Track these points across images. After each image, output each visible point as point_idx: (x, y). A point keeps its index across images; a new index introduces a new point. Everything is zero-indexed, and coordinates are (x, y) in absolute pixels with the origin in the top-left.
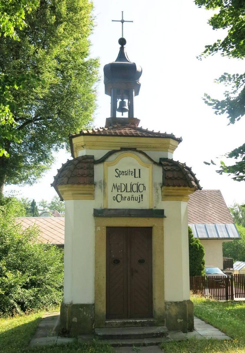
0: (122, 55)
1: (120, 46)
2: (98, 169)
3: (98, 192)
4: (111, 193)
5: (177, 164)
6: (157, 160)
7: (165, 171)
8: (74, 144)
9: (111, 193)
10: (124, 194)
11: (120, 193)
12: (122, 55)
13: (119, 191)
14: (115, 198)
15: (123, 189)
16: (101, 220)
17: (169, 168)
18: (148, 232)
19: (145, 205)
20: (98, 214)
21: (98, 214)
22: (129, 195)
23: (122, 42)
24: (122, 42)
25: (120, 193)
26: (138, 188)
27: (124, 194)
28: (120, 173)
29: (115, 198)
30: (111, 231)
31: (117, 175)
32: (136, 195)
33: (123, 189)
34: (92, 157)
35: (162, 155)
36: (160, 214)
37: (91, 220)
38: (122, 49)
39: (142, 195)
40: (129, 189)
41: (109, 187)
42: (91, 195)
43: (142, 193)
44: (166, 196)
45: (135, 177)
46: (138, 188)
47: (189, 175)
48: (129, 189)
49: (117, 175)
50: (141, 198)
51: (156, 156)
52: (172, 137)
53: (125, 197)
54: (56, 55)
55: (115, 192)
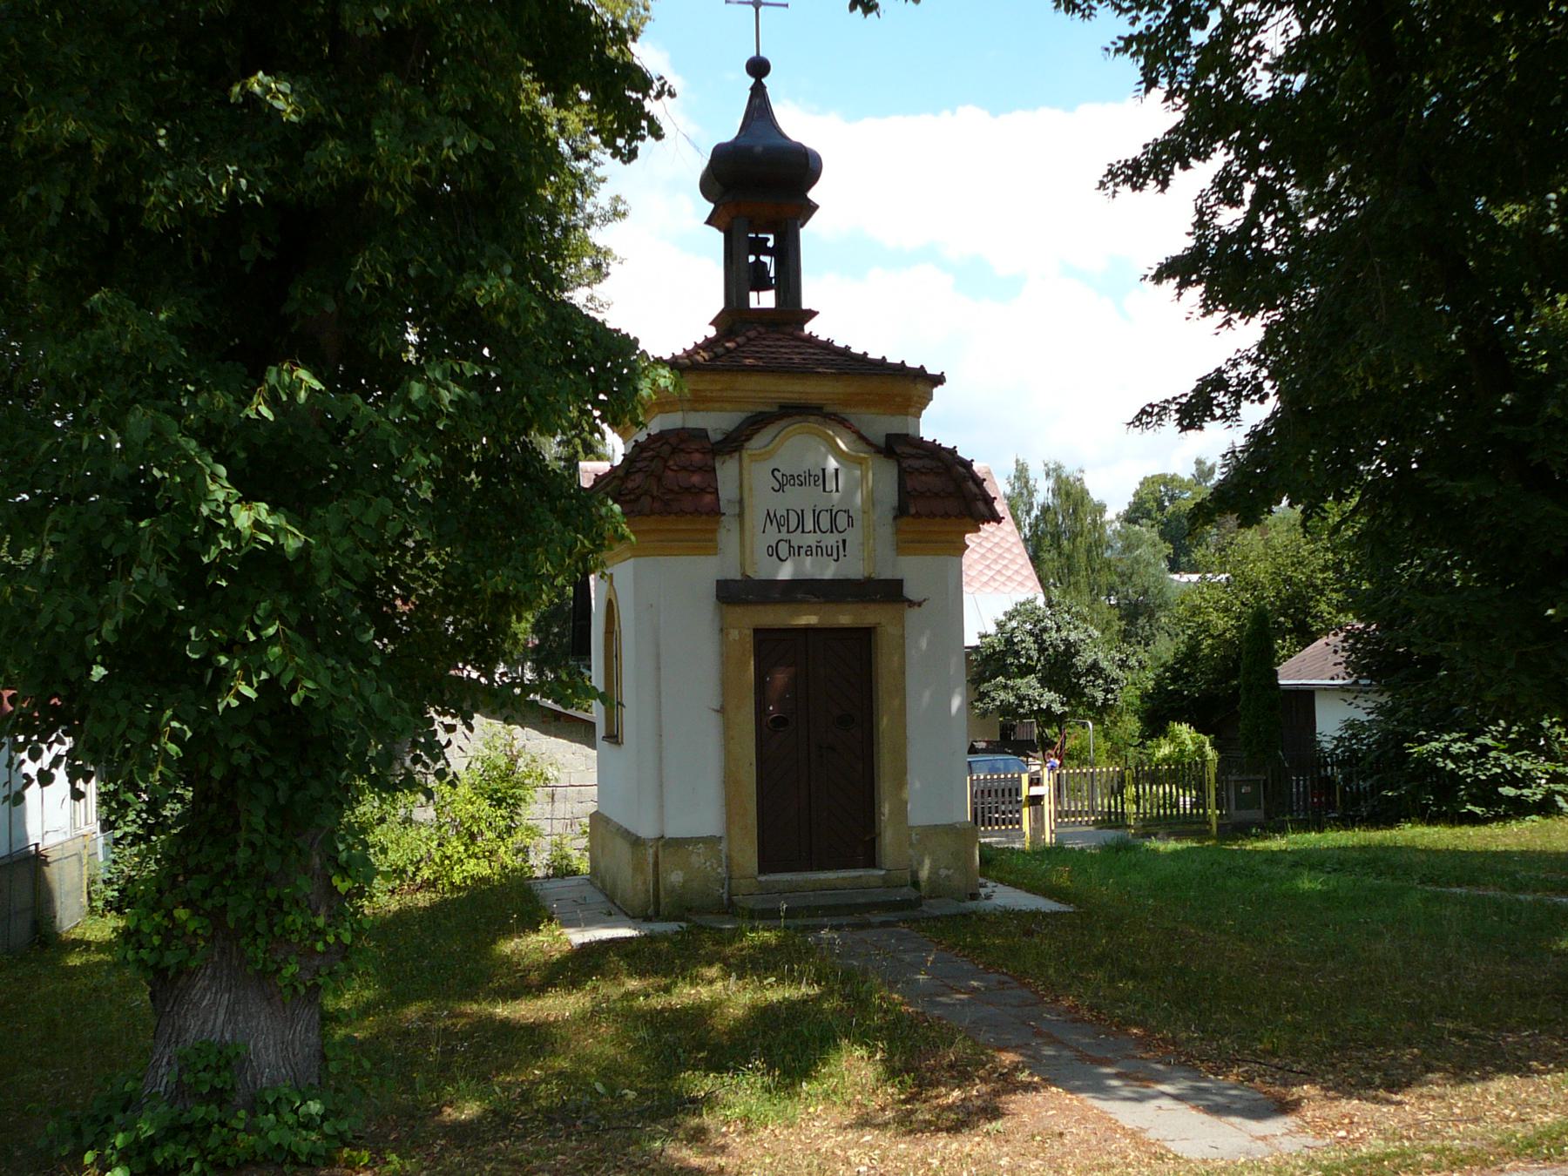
0: (759, 106)
1: (752, 81)
2: (727, 472)
3: (728, 536)
4: (763, 537)
5: (934, 450)
6: (880, 441)
7: (903, 474)
8: (743, 574)
9: (763, 537)
10: (797, 539)
11: (784, 535)
12: (759, 106)
13: (784, 529)
14: (773, 551)
15: (793, 525)
16: (738, 612)
17: (917, 464)
18: (864, 638)
19: (853, 568)
20: (732, 593)
21: (732, 593)
22: (811, 540)
23: (758, 68)
24: (758, 68)
25: (784, 535)
26: (833, 520)
27: (797, 539)
28: (783, 482)
29: (773, 551)
30: (769, 644)
31: (777, 487)
32: (831, 540)
33: (793, 525)
34: (702, 434)
35: (894, 425)
36: (890, 592)
37: (705, 609)
38: (758, 92)
39: (844, 541)
40: (809, 525)
41: (756, 517)
42: (707, 546)
43: (843, 536)
44: (904, 546)
45: (824, 490)
46: (833, 520)
47: (970, 483)
48: (809, 525)
49: (777, 487)
50: (841, 548)
51: (881, 425)
52: (920, 374)
53: (799, 547)
54: (461, 728)
55: (772, 535)
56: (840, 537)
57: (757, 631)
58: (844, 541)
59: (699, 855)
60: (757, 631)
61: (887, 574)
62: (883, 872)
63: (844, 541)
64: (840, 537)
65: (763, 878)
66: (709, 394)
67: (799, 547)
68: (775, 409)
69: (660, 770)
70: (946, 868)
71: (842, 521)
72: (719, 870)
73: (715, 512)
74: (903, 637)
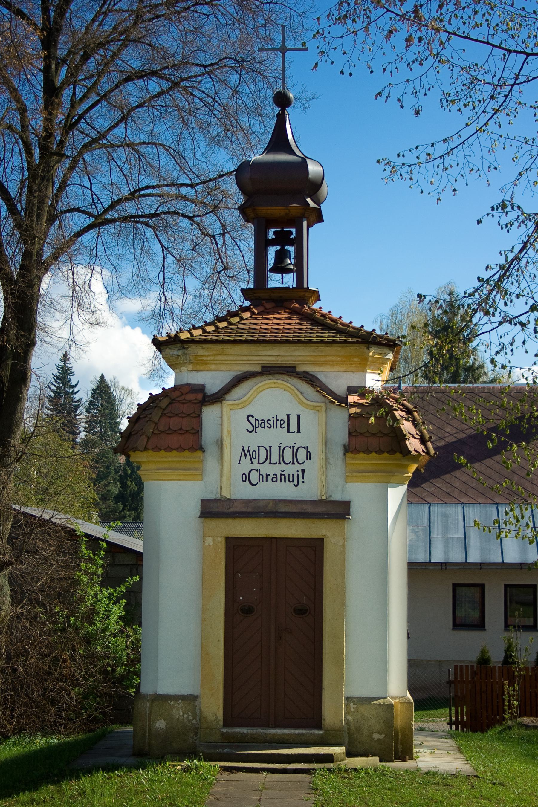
10: (266, 469)
13: (255, 461)
14: (246, 478)
15: (263, 458)
22: (276, 469)
25: (255, 466)
26: (295, 455)
27: (266, 469)
29: (246, 478)
31: (251, 430)
32: (292, 470)
33: (263, 458)
40: (275, 458)
45: (288, 432)
46: (295, 455)
48: (275, 458)
49: (251, 429)
53: (267, 475)
55: (246, 465)
56: (299, 468)
57: (228, 539)
58: (303, 471)
59: (178, 708)
60: (228, 539)
61: (337, 496)
62: (321, 732)
63: (303, 471)
64: (299, 468)
65: (225, 730)
66: (205, 358)
67: (267, 475)
68: (258, 369)
69: (326, 430)
70: (378, 733)
71: (302, 455)
72: (194, 721)
73: (202, 449)
74: (344, 546)
